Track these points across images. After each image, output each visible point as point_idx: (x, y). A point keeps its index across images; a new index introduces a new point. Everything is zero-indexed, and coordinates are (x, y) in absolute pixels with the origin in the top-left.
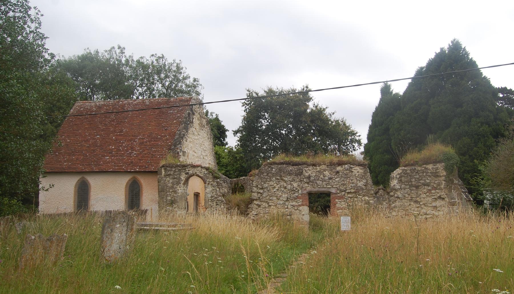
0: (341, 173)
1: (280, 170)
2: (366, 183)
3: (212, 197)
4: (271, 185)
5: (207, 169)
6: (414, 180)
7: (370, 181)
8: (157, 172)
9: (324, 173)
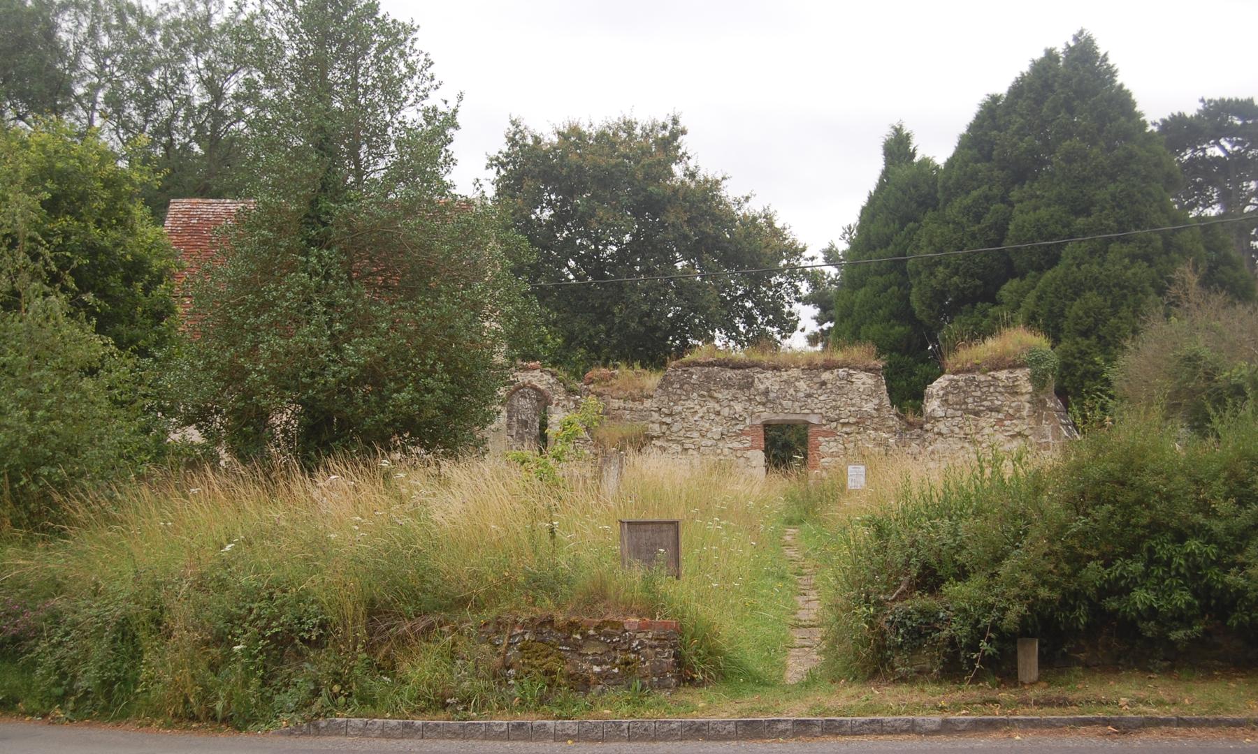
0: (829, 386)
1: (708, 377)
2: (880, 404)
6: (970, 400)
7: (887, 402)
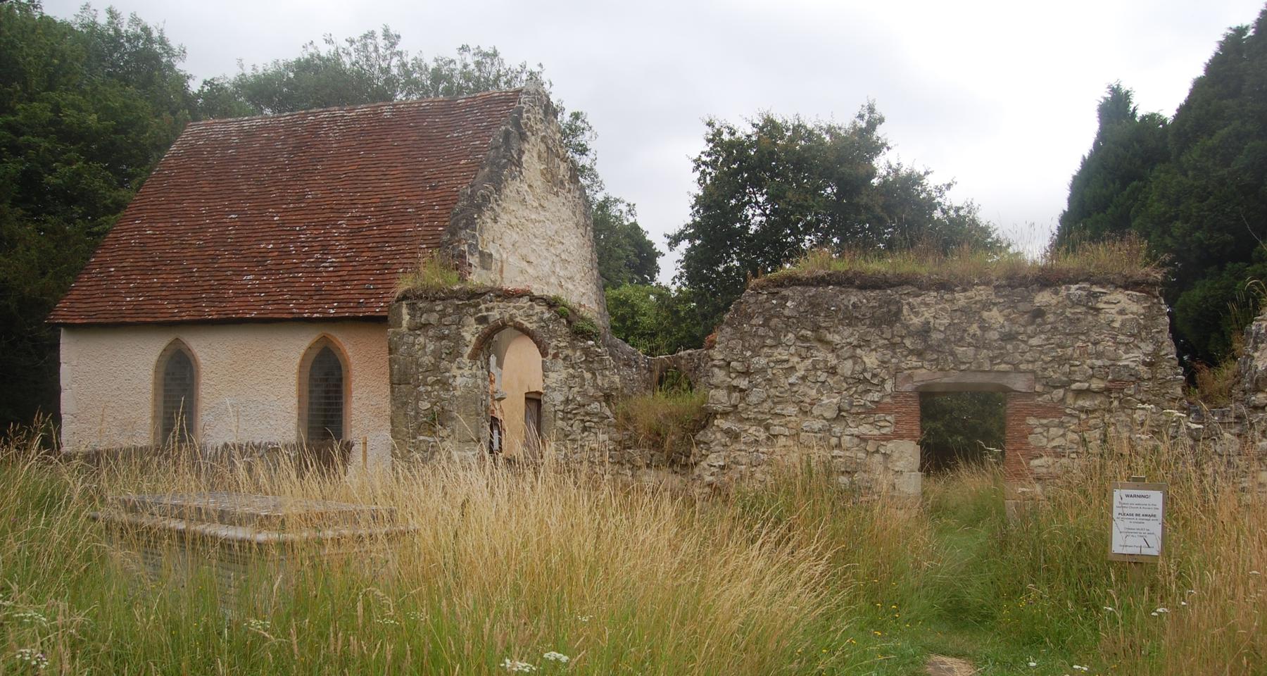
0: (1050, 318)
1: (814, 305)
2: (1155, 354)
3: (567, 401)
4: (777, 362)
5: (552, 303)
8: (386, 318)
9: (985, 314)
